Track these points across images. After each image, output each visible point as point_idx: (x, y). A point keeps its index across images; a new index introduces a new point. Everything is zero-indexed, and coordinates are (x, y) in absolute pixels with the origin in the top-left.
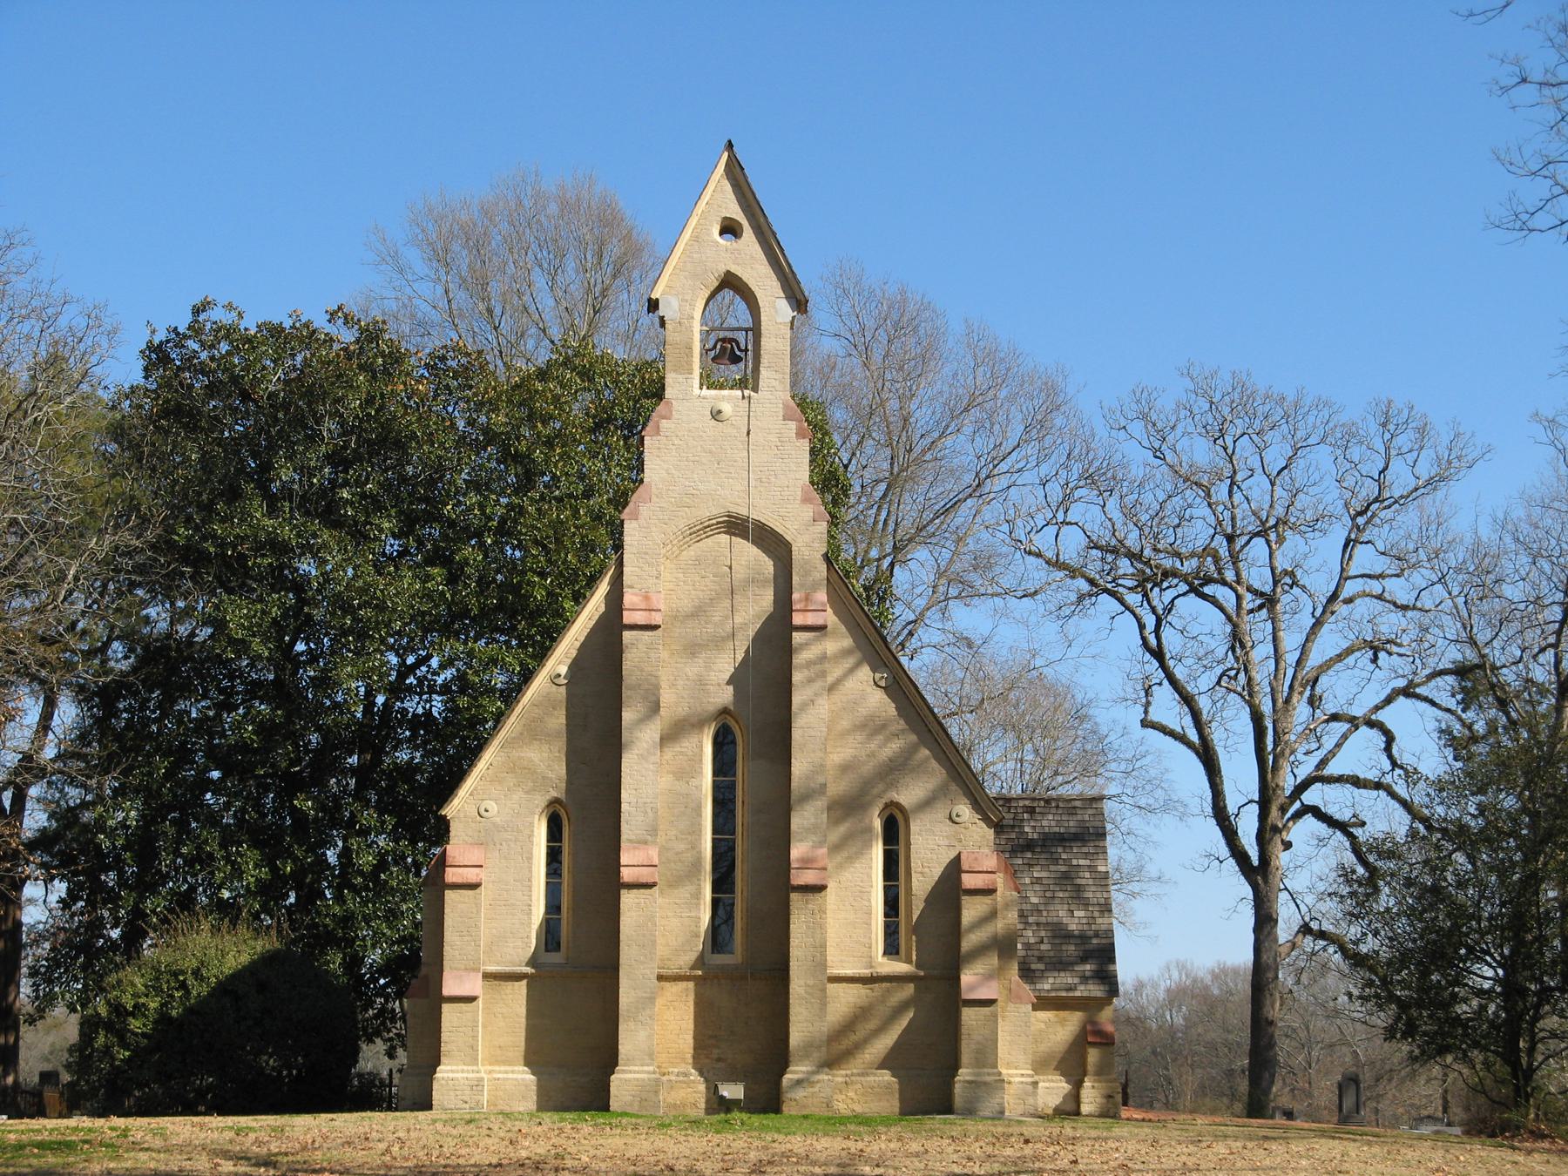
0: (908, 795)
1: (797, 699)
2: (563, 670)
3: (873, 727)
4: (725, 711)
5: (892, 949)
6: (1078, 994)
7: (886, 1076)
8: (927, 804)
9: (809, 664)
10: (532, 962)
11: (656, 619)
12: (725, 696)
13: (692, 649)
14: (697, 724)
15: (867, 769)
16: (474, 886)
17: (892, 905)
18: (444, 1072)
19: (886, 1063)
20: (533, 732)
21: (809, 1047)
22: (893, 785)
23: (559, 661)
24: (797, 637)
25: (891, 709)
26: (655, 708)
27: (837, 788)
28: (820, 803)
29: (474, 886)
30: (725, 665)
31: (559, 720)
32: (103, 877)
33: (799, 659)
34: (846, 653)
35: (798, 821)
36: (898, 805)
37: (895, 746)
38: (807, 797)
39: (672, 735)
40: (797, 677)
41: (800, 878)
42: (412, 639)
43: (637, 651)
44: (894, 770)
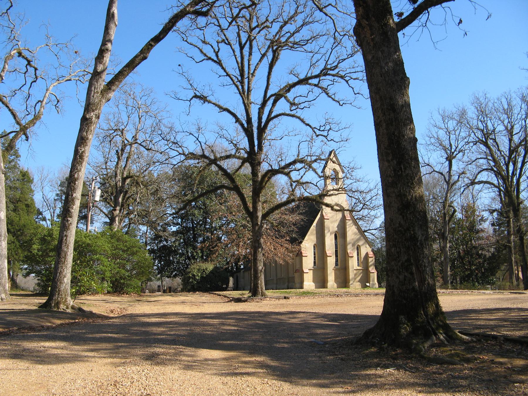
0: (360, 243)
1: (347, 230)
2: (315, 225)
3: (355, 234)
4: (336, 231)
5: (358, 265)
6: (520, 275)
7: (359, 283)
8: (363, 245)
9: (349, 225)
10: (313, 267)
11: (329, 218)
12: (336, 229)
13: (332, 222)
14: (333, 233)
15: (355, 240)
16: (306, 256)
17: (358, 260)
18: (305, 283)
19: (359, 281)
20: (312, 234)
21: (352, 279)
22: (358, 242)
23: (315, 224)
24: (347, 221)
25: (357, 231)
26: (329, 231)
27: (352, 242)
28: (351, 245)
29: (306, 256)
30: (336, 224)
31: (315, 232)
32: (506, 264)
33: (347, 224)
34: (351, 223)
35: (348, 247)
36: (358, 245)
37: (358, 237)
38: (349, 243)
39: (331, 234)
40: (347, 227)
41: (350, 255)
42: (234, 216)
43: (327, 223)
44: (358, 240)
